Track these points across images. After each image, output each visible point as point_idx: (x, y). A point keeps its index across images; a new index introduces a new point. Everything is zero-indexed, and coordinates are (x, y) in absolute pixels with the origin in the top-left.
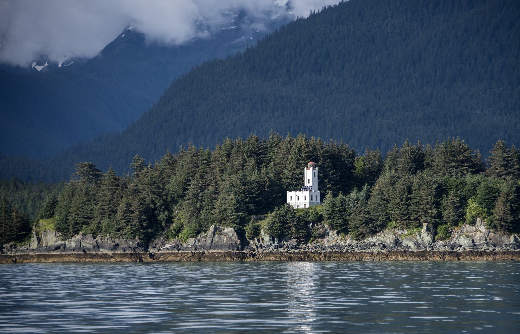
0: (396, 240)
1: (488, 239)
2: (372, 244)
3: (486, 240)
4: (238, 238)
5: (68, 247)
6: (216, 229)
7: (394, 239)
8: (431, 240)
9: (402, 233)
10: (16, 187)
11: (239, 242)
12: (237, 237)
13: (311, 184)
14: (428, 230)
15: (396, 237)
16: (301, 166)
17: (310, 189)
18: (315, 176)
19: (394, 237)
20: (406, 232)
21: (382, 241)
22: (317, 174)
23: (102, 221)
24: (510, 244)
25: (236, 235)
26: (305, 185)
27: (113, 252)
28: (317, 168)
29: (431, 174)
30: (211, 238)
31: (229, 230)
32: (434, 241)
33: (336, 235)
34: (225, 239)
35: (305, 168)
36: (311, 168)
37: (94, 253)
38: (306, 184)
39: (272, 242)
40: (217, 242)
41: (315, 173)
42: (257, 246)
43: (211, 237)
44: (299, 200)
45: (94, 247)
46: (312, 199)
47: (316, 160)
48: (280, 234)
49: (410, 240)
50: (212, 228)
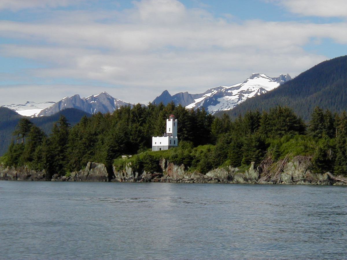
0: (229, 176)
1: (305, 177)
2: (210, 178)
3: (304, 177)
4: (108, 172)
6: (91, 165)
7: (228, 175)
8: (257, 177)
10: (24, 146)
11: (107, 175)
12: (106, 171)
13: (171, 132)
14: (255, 168)
15: (229, 173)
16: (165, 117)
17: (170, 135)
19: (228, 173)
20: (237, 169)
21: (218, 177)
22: (176, 124)
24: (324, 181)
25: (106, 170)
26: (167, 132)
30: (87, 172)
32: (259, 177)
33: (183, 171)
34: (97, 173)
35: (168, 120)
36: (172, 120)
38: (168, 132)
40: (91, 175)
41: (174, 123)
42: (121, 179)
43: (87, 171)
44: (160, 142)
45: (14, 177)
47: (176, 117)
48: (138, 168)
49: (241, 176)
50: (88, 164)
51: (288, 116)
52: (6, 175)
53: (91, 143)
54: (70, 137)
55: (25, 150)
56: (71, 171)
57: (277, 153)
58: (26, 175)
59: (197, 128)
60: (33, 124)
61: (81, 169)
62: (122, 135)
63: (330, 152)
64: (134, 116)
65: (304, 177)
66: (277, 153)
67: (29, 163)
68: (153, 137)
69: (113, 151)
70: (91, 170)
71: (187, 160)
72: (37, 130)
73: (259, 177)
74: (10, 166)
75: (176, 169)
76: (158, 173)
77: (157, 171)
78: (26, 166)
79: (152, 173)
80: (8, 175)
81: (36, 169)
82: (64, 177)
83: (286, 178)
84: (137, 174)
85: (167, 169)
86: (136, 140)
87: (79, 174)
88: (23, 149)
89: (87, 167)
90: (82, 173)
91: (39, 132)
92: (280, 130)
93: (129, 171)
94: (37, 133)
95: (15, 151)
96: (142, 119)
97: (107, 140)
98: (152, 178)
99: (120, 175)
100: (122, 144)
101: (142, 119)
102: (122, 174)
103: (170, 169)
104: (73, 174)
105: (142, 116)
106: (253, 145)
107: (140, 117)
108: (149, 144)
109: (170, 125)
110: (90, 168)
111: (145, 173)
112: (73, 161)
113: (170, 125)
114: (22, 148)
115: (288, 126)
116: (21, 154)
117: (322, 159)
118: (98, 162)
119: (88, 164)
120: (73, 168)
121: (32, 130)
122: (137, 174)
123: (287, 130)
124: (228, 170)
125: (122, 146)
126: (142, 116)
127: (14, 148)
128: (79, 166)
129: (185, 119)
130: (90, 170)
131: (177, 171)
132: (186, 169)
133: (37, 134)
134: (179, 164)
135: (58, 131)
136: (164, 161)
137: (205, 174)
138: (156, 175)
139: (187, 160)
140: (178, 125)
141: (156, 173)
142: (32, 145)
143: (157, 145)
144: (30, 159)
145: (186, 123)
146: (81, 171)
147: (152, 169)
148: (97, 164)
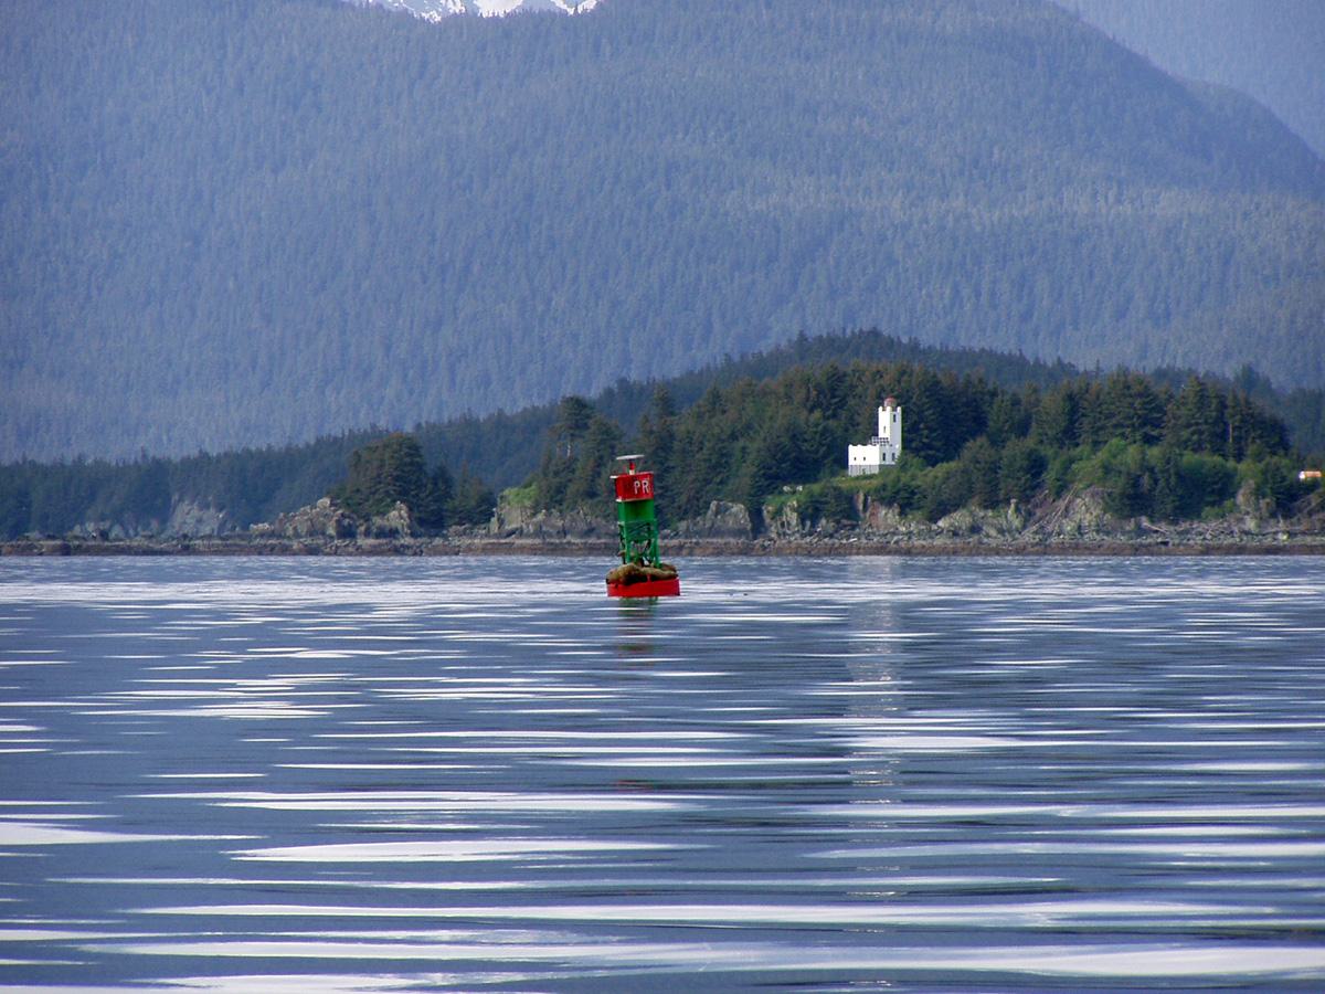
4: (751, 521)
5: (525, 531)
6: (718, 506)
9: (331, 537)
11: (749, 527)
14: (1017, 510)
17: (885, 441)
18: (895, 421)
22: (899, 418)
23: (570, 484)
27: (583, 541)
28: (899, 409)
29: (721, 425)
31: (738, 509)
35: (881, 408)
36: (889, 408)
37: (557, 541)
38: (881, 434)
39: (800, 526)
44: (864, 457)
45: (558, 532)
46: (884, 459)
47: (902, 400)
51: (1140, 395)
52: (541, 527)
53: (721, 464)
54: (676, 445)
55: (577, 473)
56: (681, 519)
57: (1059, 483)
58: (586, 528)
59: (950, 417)
60: (592, 408)
61: (700, 514)
62: (785, 440)
63: (1146, 480)
64: (819, 393)
65: (1098, 525)
66: (1059, 483)
67: (590, 501)
68: (851, 447)
69: (767, 476)
70: (719, 517)
71: (1189, 458)
72: (604, 429)
73: (1024, 527)
74: (547, 509)
75: (884, 512)
76: (849, 522)
77: (848, 518)
78: (584, 508)
79: (838, 522)
80: (544, 529)
81: (606, 517)
82: (666, 531)
83: (1069, 528)
84: (808, 523)
85: (868, 514)
86: (817, 452)
87: (695, 525)
88: (573, 471)
89: (710, 512)
90: (701, 523)
91: (607, 432)
92: (1122, 426)
93: (793, 518)
94: (603, 433)
95: (556, 474)
96: (836, 400)
97: (753, 447)
98: (836, 532)
99: (776, 527)
100: (785, 462)
101: (836, 400)
102: (779, 523)
103: (872, 514)
104: (683, 525)
105: (837, 393)
106: (1018, 465)
107: (834, 397)
108: (842, 461)
109: (888, 421)
110: (717, 514)
111: (824, 521)
112: (683, 499)
113: (888, 421)
114: (570, 466)
115: (1139, 417)
116: (570, 481)
117: (1131, 491)
118: (732, 501)
119: (713, 505)
120: (686, 512)
121: (593, 428)
122: (808, 523)
123: (1137, 425)
124: (972, 514)
125: (783, 465)
126: (837, 393)
127: (552, 468)
128: (695, 508)
129: (924, 404)
130: (716, 516)
131: (887, 516)
132: (902, 514)
133: (605, 437)
134: (889, 504)
135: (651, 432)
136: (862, 498)
137: (935, 523)
138: (845, 526)
139: (904, 494)
140: (903, 422)
141: (845, 522)
142: (596, 461)
143: (860, 462)
144: (592, 494)
145: (926, 413)
146: (698, 518)
147: (839, 514)
148: (730, 504)
